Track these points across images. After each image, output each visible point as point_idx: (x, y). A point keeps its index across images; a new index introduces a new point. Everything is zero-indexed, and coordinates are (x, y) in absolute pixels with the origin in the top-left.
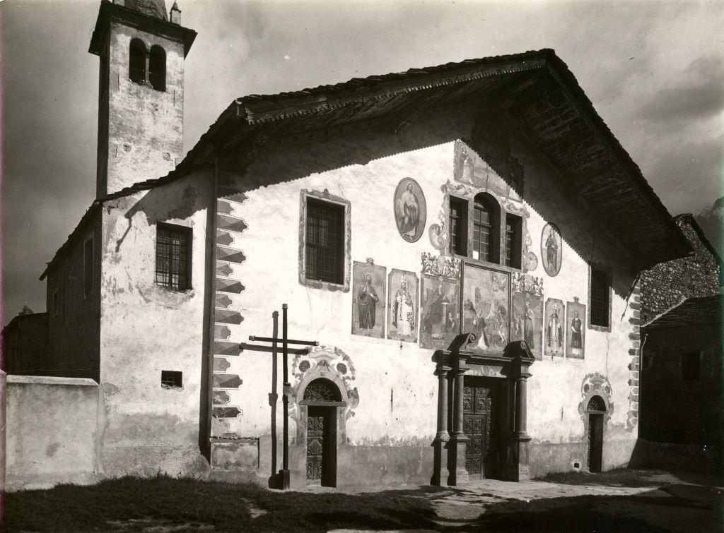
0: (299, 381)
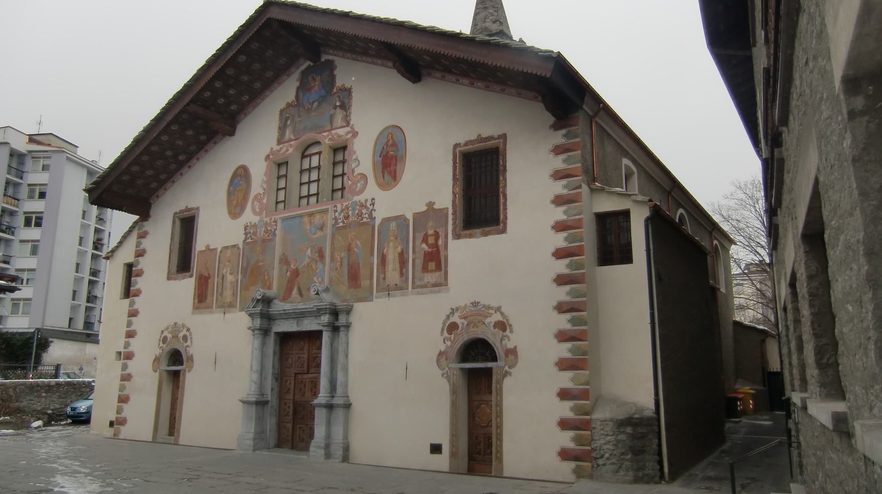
0: (161, 352)
